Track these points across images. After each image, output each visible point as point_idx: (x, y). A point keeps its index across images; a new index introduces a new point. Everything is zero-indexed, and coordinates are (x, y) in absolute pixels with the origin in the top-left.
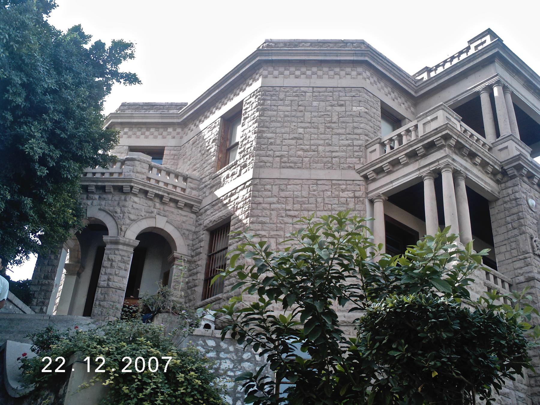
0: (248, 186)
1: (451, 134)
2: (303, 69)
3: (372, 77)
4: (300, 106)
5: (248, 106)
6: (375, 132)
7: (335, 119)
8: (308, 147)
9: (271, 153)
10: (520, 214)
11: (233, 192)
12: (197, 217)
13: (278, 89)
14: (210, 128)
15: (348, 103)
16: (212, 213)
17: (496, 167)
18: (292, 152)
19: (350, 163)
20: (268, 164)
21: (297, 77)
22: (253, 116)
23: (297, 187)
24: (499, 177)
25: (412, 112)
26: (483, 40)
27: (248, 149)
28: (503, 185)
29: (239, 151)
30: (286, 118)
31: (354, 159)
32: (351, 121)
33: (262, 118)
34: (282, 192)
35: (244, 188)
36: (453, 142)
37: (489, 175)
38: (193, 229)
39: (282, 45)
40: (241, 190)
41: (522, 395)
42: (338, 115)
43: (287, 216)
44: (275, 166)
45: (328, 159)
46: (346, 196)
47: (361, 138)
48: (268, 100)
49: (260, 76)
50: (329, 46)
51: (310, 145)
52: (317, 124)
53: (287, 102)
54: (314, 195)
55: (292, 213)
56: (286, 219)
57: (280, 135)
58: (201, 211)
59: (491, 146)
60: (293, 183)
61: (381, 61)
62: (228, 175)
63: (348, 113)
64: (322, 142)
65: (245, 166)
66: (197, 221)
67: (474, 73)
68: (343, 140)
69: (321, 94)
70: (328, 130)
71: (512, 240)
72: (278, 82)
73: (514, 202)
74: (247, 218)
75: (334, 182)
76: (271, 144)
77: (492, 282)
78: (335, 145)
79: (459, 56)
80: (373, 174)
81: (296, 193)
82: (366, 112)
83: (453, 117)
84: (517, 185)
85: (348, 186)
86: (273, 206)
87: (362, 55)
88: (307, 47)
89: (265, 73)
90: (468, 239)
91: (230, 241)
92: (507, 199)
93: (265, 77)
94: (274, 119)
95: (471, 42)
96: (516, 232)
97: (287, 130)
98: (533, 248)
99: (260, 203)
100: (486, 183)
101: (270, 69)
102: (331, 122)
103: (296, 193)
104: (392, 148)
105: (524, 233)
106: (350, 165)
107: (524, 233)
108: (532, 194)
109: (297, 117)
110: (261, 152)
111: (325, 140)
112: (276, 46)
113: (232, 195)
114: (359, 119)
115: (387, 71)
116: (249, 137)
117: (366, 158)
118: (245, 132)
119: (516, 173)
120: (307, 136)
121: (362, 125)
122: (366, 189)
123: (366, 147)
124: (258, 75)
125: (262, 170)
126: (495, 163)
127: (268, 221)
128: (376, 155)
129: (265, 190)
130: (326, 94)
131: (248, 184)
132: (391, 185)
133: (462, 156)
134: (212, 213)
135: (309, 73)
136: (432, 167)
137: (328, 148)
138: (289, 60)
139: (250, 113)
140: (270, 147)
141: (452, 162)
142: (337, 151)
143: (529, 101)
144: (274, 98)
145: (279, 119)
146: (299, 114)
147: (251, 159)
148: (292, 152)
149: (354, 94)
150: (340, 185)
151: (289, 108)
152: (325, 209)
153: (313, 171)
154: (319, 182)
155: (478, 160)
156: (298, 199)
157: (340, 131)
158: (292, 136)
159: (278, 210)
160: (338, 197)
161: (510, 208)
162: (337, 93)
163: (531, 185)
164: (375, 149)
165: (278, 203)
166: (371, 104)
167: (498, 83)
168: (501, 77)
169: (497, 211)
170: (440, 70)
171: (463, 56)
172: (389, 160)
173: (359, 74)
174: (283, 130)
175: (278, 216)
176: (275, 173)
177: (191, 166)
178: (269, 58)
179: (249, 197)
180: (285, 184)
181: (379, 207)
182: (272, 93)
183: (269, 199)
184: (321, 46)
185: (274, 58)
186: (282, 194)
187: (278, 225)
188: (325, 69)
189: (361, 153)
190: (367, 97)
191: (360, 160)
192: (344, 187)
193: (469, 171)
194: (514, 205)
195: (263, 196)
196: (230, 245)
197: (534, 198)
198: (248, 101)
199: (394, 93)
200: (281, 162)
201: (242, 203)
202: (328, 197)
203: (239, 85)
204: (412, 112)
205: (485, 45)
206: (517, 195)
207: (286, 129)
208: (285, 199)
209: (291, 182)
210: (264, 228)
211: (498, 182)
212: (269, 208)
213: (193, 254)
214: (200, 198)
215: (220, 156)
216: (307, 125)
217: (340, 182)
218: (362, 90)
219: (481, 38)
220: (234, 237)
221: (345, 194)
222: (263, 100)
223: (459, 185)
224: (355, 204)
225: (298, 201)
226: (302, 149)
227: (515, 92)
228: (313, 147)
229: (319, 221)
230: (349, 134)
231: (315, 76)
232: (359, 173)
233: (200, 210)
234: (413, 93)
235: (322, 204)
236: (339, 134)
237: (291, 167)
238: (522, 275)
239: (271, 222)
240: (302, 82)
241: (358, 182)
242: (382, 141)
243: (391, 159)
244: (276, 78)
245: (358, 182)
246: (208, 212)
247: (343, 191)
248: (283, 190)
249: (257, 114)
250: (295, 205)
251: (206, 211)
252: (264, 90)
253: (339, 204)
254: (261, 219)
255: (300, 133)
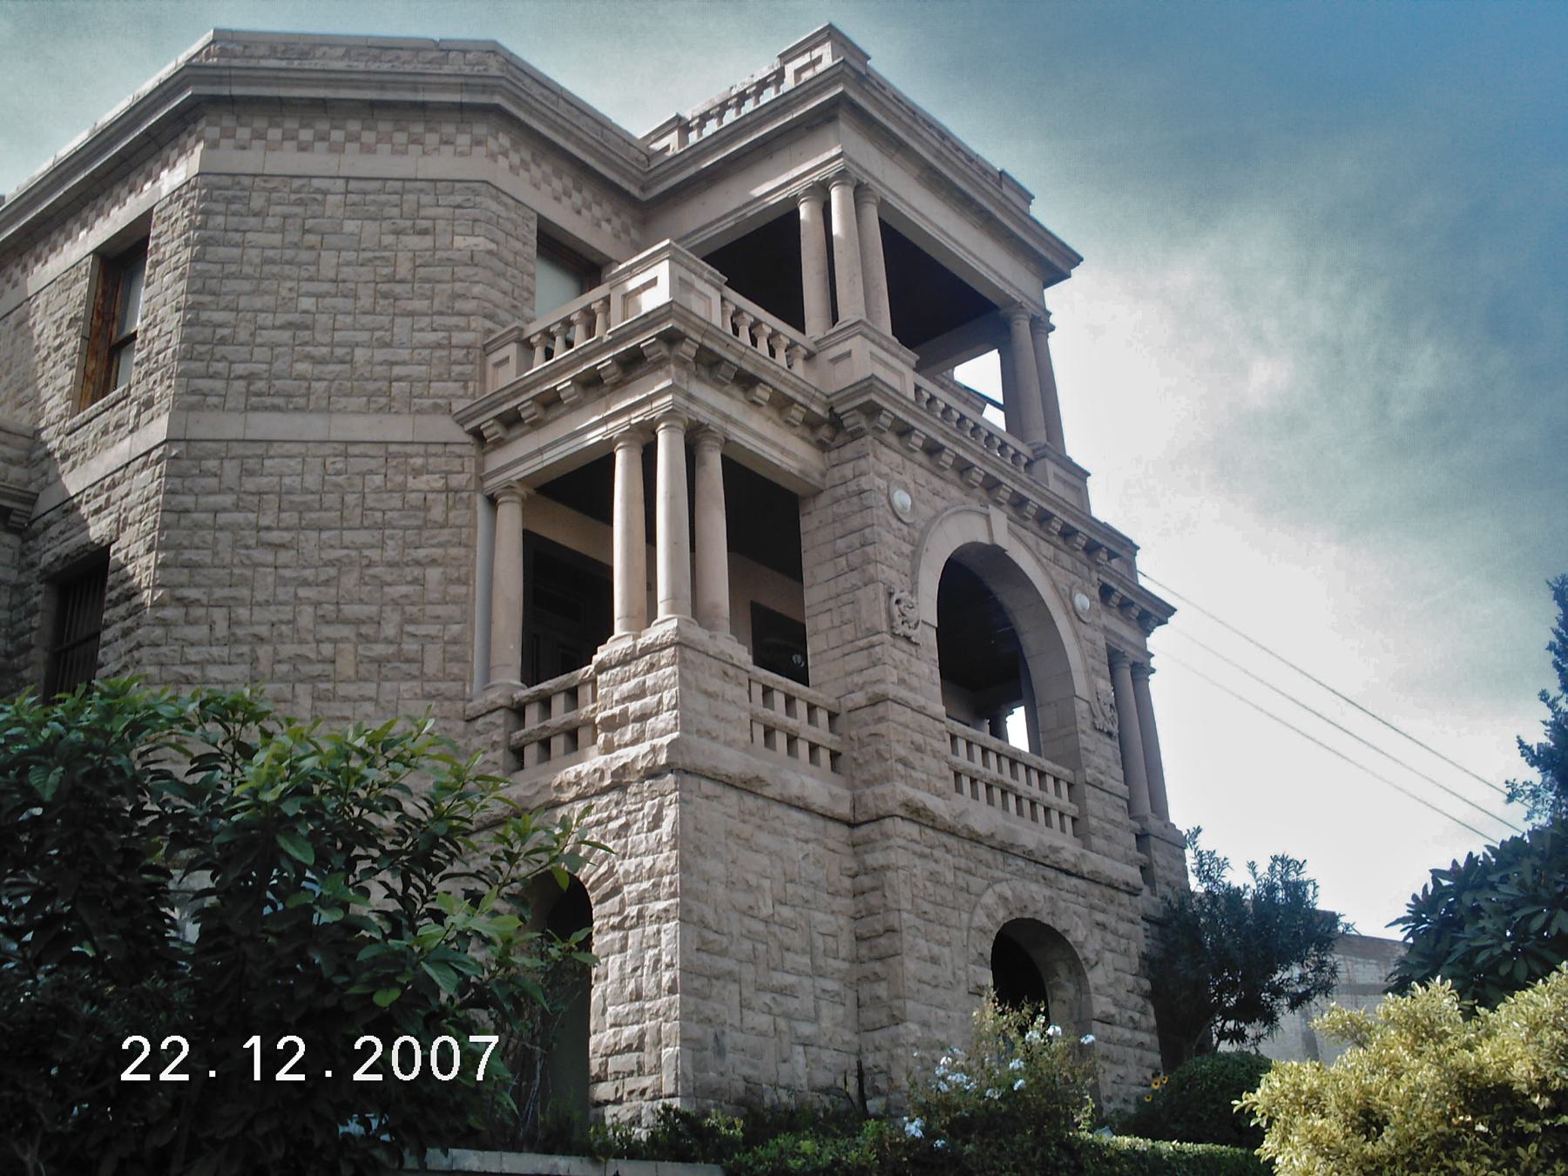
0: (158, 461)
1: (682, 328)
2: (323, 126)
3: (517, 151)
4: (309, 231)
5: (164, 227)
6: (514, 307)
7: (403, 270)
8: (324, 350)
9: (220, 366)
10: (867, 531)
11: (118, 475)
12: (24, 541)
13: (246, 181)
14: (63, 282)
15: (441, 224)
16: (62, 533)
17: (815, 408)
18: (279, 366)
19: (436, 396)
20: (212, 400)
21: (303, 148)
22: (174, 259)
23: (292, 463)
24: (824, 433)
25: (632, 241)
26: (816, 53)
27: (158, 353)
28: (834, 455)
29: (137, 357)
30: (266, 268)
31: (450, 384)
32: (447, 277)
33: (199, 266)
34: (251, 479)
35: (145, 466)
36: (687, 350)
37: (798, 430)
38: (13, 576)
39: (262, 50)
40: (138, 471)
41: (830, 985)
42: (413, 260)
43: (262, 544)
44: (230, 405)
45: (378, 384)
46: (423, 486)
47: (473, 325)
48: (218, 214)
49: (198, 141)
50: (398, 58)
51: (333, 345)
52: (352, 286)
53: (271, 222)
54: (337, 485)
55: (274, 536)
56: (259, 555)
57: (249, 316)
58: (35, 526)
59: (813, 348)
60: (280, 451)
61: (538, 106)
62: (107, 426)
63: (439, 254)
64: (363, 336)
65: (148, 404)
66: (23, 554)
67: (790, 143)
68: (422, 330)
69: (369, 198)
70: (382, 302)
71: (845, 598)
72: (250, 161)
73: (855, 499)
74: (149, 550)
75: (392, 448)
76: (223, 341)
77: (778, 713)
78: (402, 345)
79: (758, 94)
80: (532, 410)
81: (287, 480)
82: (490, 252)
83: (701, 277)
84: (865, 456)
85: (431, 460)
86: (223, 518)
87: (485, 89)
88: (336, 59)
89: (213, 132)
90: (716, 606)
91: (105, 616)
92: (840, 491)
93: (212, 145)
94: (233, 268)
95: (786, 57)
96: (854, 578)
97: (269, 300)
98: (891, 618)
99: (187, 511)
100: (783, 450)
101: (228, 122)
102: (392, 279)
103: (287, 480)
104: (569, 344)
105: (872, 581)
106: (439, 401)
107: (872, 581)
108: (907, 478)
109: (300, 265)
110: (194, 365)
111: (373, 330)
112: (248, 52)
113: (114, 485)
114: (470, 271)
115: (557, 131)
116: (162, 321)
117: (483, 380)
118: (157, 304)
119: (864, 424)
120: (323, 319)
121: (477, 290)
122: (480, 466)
123: (486, 350)
124: (193, 138)
125: (193, 416)
126: (813, 399)
127: (208, 560)
128: (507, 377)
129: (203, 473)
130: (383, 198)
131: (155, 455)
132: (538, 459)
133: (719, 384)
134: (62, 533)
135: (337, 135)
136: (636, 417)
137: (380, 355)
138: (280, 99)
139: (169, 249)
140: (220, 350)
141: (686, 403)
142: (404, 363)
143: (931, 223)
144: (234, 207)
145: (247, 270)
146: (305, 256)
147: (167, 383)
148: (279, 366)
149: (458, 199)
150: (408, 456)
151: (276, 239)
152: (366, 523)
153: (338, 420)
154: (353, 450)
155: (762, 393)
156: (292, 497)
157: (420, 305)
158: (281, 319)
159: (233, 527)
160: (403, 489)
161: (847, 516)
162: (411, 197)
163: (904, 452)
164: (507, 359)
165: (237, 507)
166: (509, 226)
167: (842, 176)
168: (850, 160)
169: (817, 523)
170: (712, 127)
171: (769, 95)
172: (533, 393)
173: (478, 142)
174: (258, 302)
175: (235, 544)
176: (231, 426)
177: (12, 391)
178: (210, 98)
179: (157, 492)
180: (258, 456)
181: (510, 520)
182: (230, 193)
183: (212, 499)
184: (376, 59)
185: (238, 91)
186: (250, 484)
187: (237, 571)
188: (385, 127)
189: (470, 367)
190: (494, 206)
191: (465, 387)
192: (419, 461)
193: (735, 423)
194: (856, 508)
195: (196, 490)
196: (107, 627)
197: (912, 486)
198: (163, 214)
199: (580, 191)
200: (248, 394)
201: (140, 508)
202: (377, 490)
203: (144, 161)
204: (632, 241)
205: (820, 68)
206: (864, 483)
207: (266, 298)
208: (256, 499)
209: (275, 449)
210: (197, 578)
211: (822, 446)
212: (210, 522)
213: (10, 647)
214: (33, 488)
215: (92, 366)
216: (326, 287)
217: (408, 449)
218: (484, 187)
219: (810, 50)
220: (116, 603)
221: (422, 482)
222: (203, 212)
223: (704, 464)
224: (448, 509)
225: (291, 502)
226: (309, 357)
227: (891, 199)
228: (339, 352)
229: (348, 556)
230: (441, 313)
231: (352, 147)
232: (461, 423)
233: (31, 523)
234: (635, 191)
235: (358, 511)
236: (412, 314)
237: (275, 408)
238: (862, 688)
239: (217, 562)
240: (318, 161)
241: (457, 449)
242: (526, 336)
243: (539, 390)
244: (244, 148)
245: (457, 449)
246: (53, 531)
247: (417, 473)
248: (251, 473)
249: (186, 254)
250: (283, 515)
251: (47, 526)
252: (208, 183)
253: (403, 509)
254: (188, 555)
255: (305, 312)
